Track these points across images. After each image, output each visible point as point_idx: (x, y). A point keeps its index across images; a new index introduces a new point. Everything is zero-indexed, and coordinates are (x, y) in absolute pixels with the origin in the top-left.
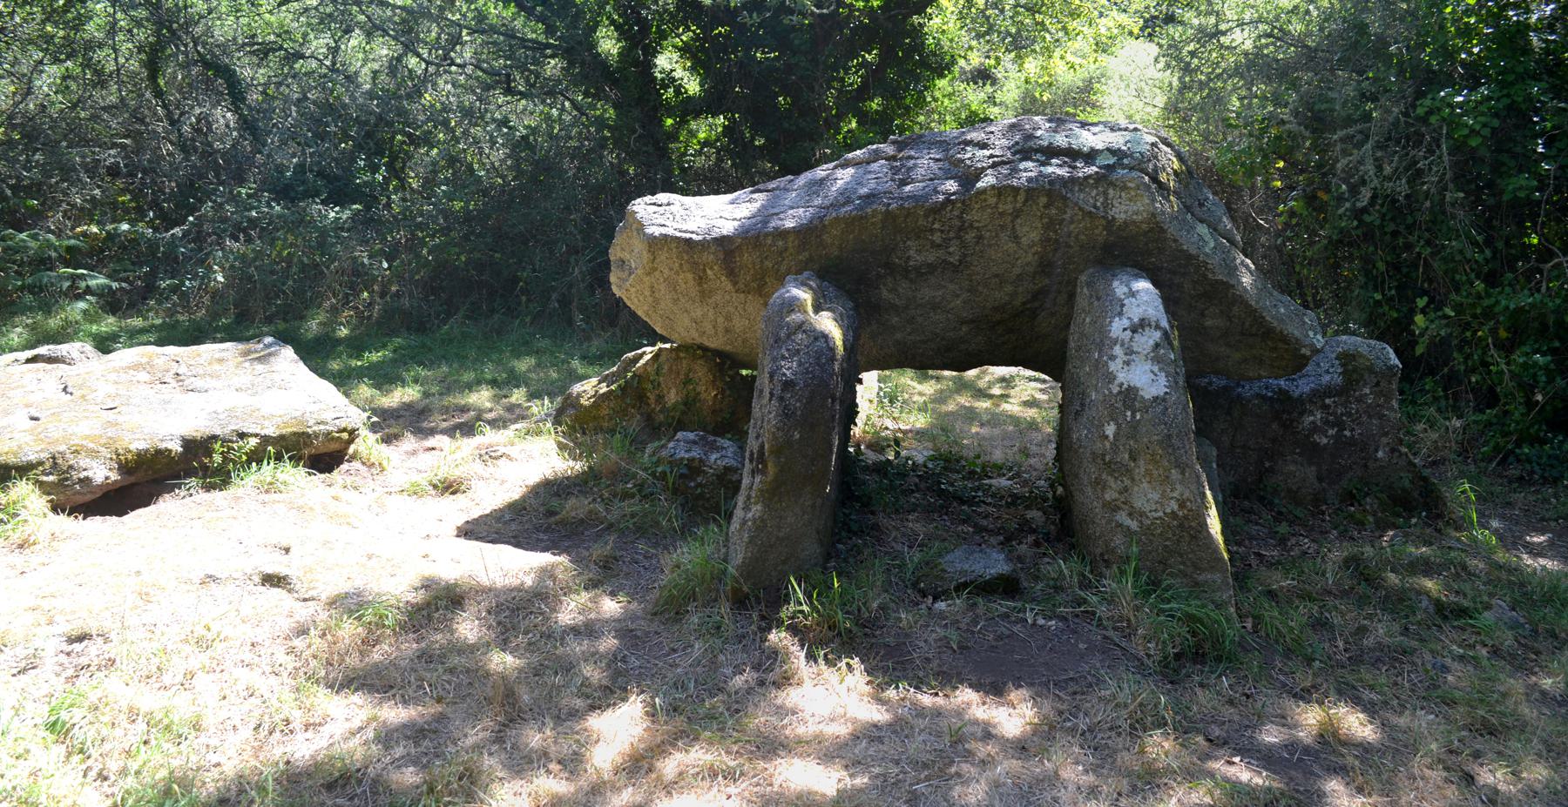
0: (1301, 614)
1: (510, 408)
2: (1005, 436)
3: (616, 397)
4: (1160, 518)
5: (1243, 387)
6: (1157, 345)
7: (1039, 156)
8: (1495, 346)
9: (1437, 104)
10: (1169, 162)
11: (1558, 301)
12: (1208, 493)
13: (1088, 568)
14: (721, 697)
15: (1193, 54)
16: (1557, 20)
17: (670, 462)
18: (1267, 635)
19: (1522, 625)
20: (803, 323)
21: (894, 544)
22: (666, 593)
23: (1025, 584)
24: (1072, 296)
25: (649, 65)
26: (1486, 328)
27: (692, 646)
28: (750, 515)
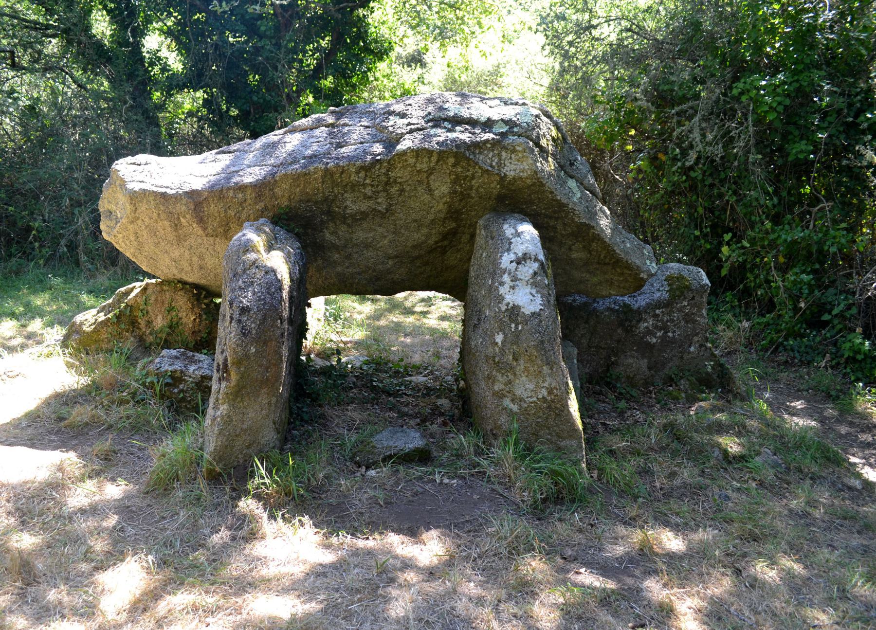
0: (631, 465)
1: (29, 336)
2: (423, 344)
3: (113, 324)
4: (535, 402)
5: (598, 303)
6: (535, 273)
7: (446, 124)
8: (775, 268)
9: (748, 86)
10: (547, 131)
11: (820, 235)
12: (570, 382)
13: (481, 440)
14: (201, 551)
15: (571, 44)
16: (836, 22)
17: (157, 374)
18: (608, 482)
19: (780, 465)
20: (256, 260)
21: (336, 429)
22: (155, 477)
23: (435, 454)
24: (473, 236)
25: (137, 47)
26: (770, 256)
27: (178, 514)
28: (219, 413)
